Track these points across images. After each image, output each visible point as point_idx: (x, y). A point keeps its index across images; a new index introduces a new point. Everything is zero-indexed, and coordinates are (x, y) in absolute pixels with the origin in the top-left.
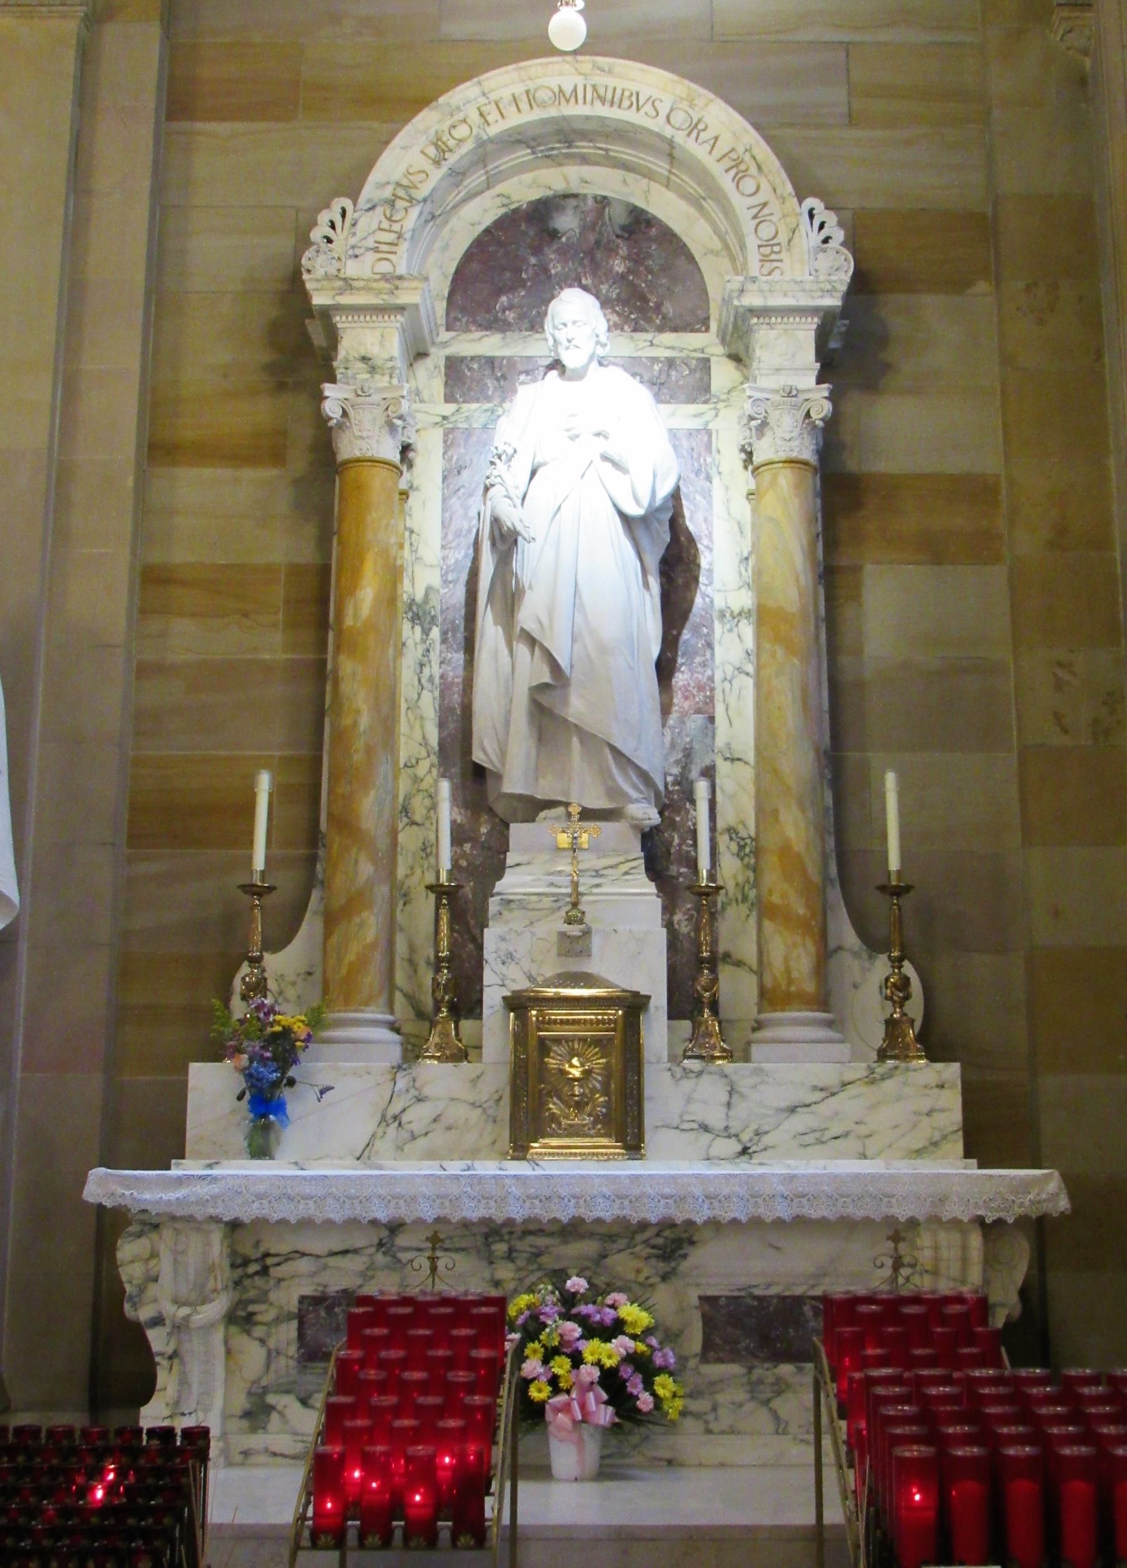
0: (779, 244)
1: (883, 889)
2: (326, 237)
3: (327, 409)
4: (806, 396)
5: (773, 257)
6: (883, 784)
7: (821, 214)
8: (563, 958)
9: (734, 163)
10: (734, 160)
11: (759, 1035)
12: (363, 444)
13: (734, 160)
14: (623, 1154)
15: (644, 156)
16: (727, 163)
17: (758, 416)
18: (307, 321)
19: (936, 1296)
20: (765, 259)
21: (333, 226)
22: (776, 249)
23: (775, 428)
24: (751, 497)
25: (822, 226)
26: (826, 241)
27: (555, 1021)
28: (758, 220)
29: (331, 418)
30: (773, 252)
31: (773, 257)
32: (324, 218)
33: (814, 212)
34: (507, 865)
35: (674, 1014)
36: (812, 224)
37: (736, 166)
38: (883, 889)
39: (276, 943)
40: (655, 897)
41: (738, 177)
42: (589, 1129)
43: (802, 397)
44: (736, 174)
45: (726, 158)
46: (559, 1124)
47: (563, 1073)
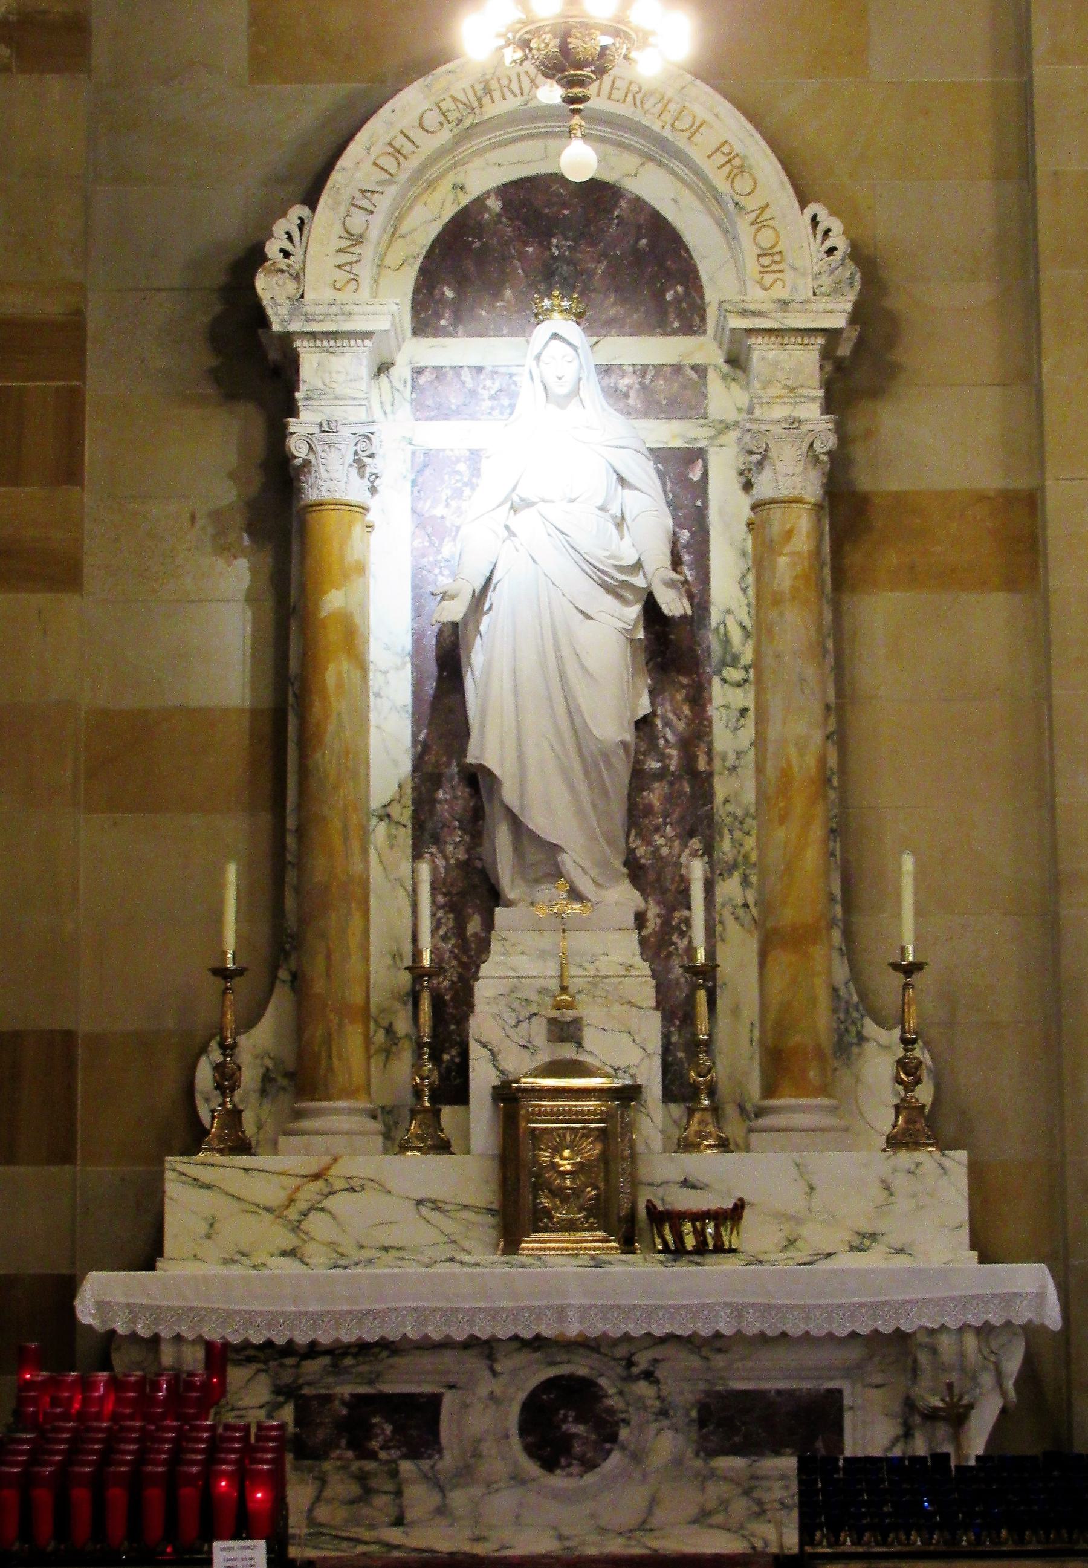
0: (780, 253)
1: (896, 966)
2: (282, 250)
3: (292, 446)
4: (811, 427)
5: (774, 267)
6: (900, 866)
7: (826, 220)
8: (551, 1043)
9: (728, 158)
10: (727, 154)
11: (761, 1122)
12: (331, 485)
13: (727, 154)
14: (616, 1248)
15: (622, 134)
16: (721, 159)
17: (757, 451)
18: (260, 331)
19: (826, 504)
20: (765, 270)
21: (290, 238)
22: (777, 258)
23: (777, 462)
24: (751, 526)
25: (827, 233)
26: (831, 251)
27: (546, 1113)
28: (756, 226)
29: (296, 457)
30: (773, 262)
31: (774, 267)
32: (280, 228)
33: (818, 219)
34: (692, 1234)
35: (668, 1096)
36: (815, 237)
37: (728, 162)
38: (896, 966)
39: (249, 1022)
40: (650, 979)
41: (732, 175)
42: (582, 1223)
43: (804, 428)
44: (730, 173)
45: (719, 153)
46: (551, 1218)
47: (554, 1166)
